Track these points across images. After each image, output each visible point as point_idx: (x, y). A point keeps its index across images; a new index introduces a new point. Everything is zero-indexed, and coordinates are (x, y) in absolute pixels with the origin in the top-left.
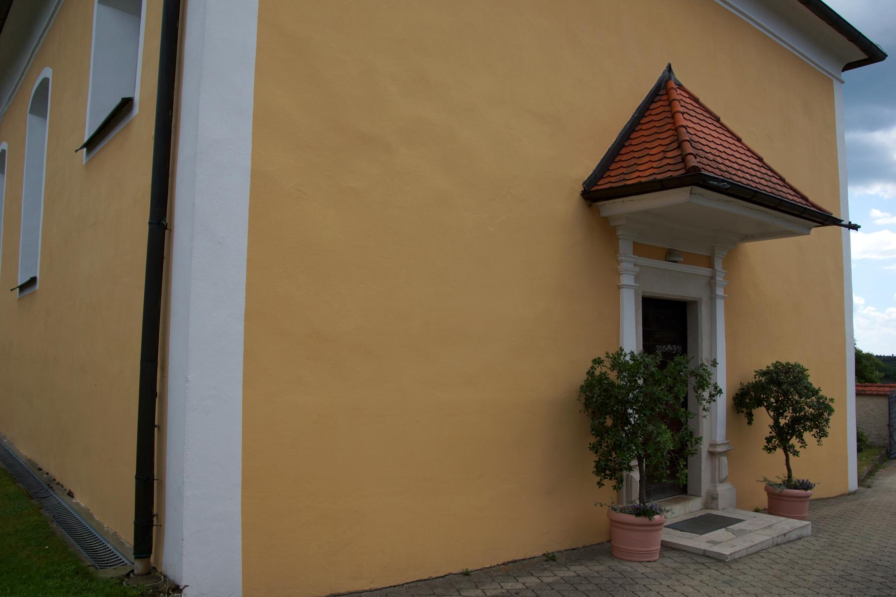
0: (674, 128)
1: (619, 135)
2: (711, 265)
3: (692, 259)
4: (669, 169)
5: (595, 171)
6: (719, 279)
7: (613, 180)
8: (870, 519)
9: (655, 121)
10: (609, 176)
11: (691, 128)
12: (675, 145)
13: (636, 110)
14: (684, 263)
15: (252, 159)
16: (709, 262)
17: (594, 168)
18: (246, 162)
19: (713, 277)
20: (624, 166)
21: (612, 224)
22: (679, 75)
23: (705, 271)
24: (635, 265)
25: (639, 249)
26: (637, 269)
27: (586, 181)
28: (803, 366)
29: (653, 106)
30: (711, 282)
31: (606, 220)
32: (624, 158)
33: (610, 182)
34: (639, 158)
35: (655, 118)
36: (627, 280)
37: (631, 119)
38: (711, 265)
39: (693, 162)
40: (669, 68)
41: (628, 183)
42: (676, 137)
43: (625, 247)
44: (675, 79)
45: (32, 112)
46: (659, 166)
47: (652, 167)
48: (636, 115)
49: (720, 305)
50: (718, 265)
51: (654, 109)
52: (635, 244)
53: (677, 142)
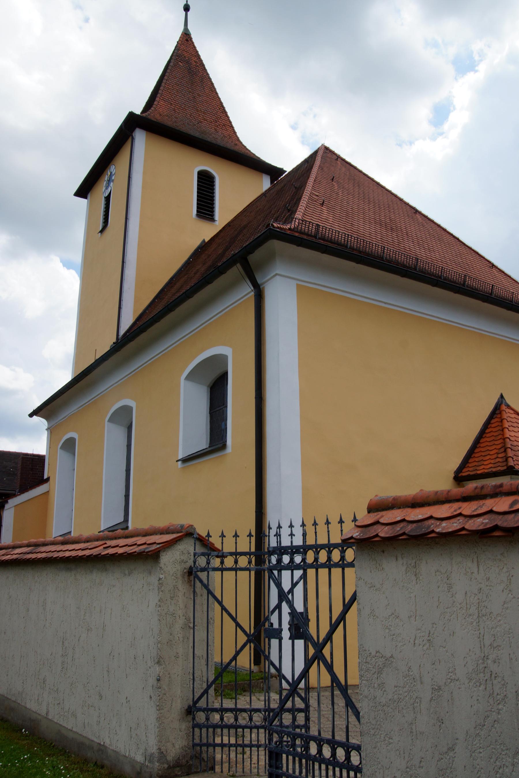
0: (503, 438)
1: (473, 441)
4: (499, 465)
5: (460, 465)
7: (470, 469)
9: (494, 432)
10: (468, 466)
11: (512, 437)
12: (503, 450)
13: (483, 425)
15: (302, 482)
17: (460, 462)
18: (299, 484)
20: (482, 451)
22: (509, 400)
27: (456, 471)
29: (493, 421)
32: (476, 455)
33: (469, 471)
34: (484, 456)
35: (494, 430)
37: (480, 431)
39: (511, 463)
40: (502, 396)
41: (479, 472)
42: (504, 445)
44: (506, 402)
45: (110, 420)
46: (494, 463)
47: (491, 463)
48: (483, 428)
51: (483, 443)
53: (503, 448)
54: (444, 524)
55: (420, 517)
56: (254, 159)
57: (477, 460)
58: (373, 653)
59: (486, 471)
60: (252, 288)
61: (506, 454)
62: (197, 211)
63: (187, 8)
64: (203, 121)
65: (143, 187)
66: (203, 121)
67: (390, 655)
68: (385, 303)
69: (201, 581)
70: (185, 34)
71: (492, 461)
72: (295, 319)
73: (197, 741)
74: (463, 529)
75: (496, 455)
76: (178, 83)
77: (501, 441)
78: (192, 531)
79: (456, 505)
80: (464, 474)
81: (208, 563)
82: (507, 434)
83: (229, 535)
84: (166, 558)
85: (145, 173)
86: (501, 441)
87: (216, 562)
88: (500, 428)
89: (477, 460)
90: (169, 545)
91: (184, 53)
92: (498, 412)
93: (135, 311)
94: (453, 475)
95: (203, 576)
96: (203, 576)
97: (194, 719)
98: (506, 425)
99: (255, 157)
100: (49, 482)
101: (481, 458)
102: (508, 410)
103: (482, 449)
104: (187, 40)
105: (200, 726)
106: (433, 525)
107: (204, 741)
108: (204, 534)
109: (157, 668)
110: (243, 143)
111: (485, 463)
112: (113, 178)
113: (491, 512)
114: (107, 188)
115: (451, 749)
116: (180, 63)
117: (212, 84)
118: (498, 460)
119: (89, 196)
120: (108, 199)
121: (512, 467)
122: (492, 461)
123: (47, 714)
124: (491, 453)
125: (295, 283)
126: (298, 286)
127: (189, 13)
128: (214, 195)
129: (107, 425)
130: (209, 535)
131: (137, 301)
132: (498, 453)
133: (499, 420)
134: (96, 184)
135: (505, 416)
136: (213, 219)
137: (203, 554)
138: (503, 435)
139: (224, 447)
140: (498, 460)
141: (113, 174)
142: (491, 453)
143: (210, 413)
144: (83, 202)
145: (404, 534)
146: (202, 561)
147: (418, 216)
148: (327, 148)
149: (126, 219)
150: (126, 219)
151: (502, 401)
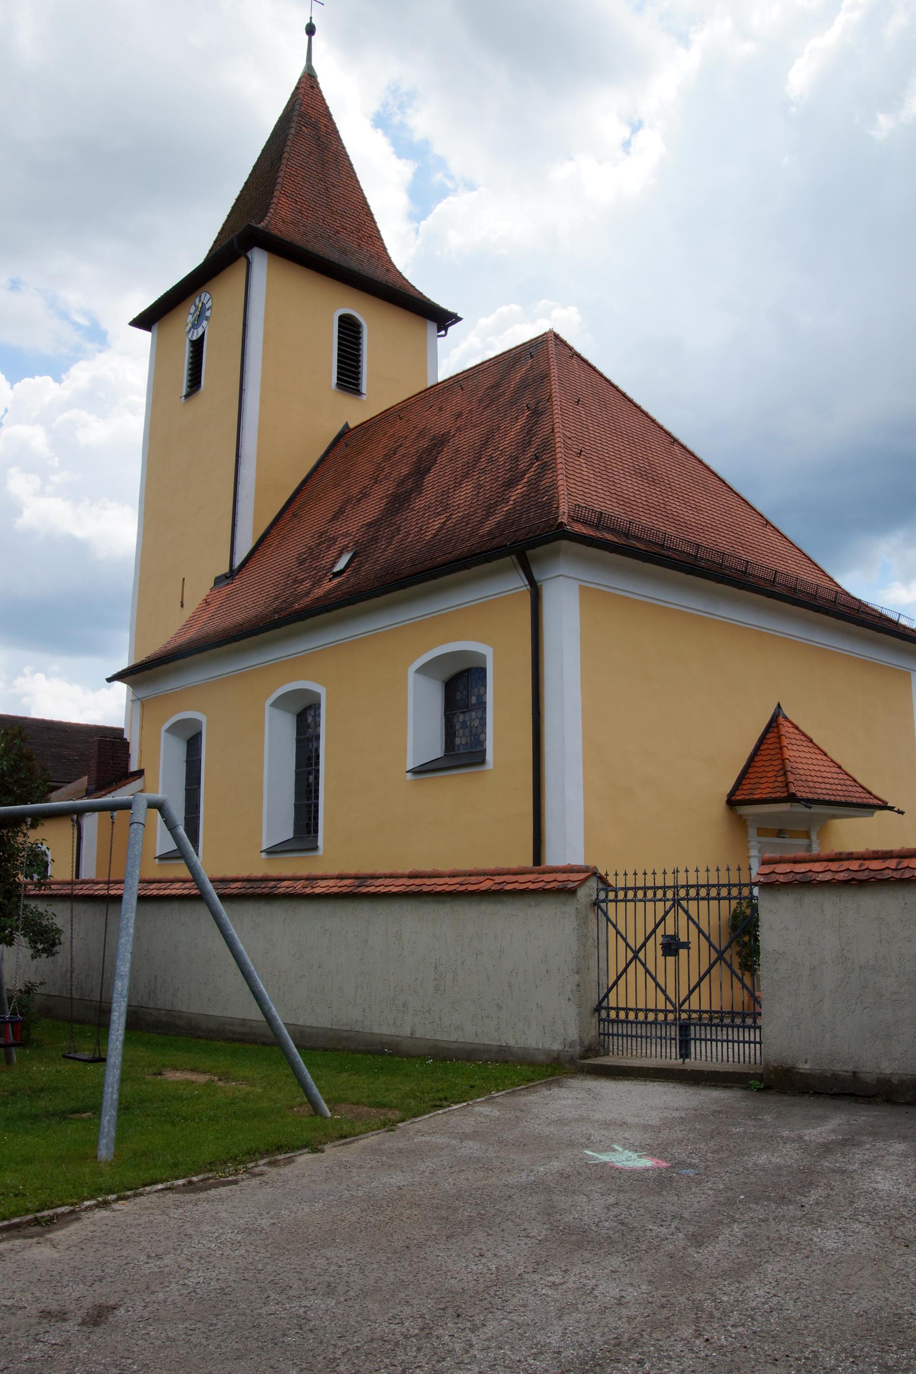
2: (809, 837)
3: (795, 834)
7: (745, 792)
12: (781, 772)
14: (790, 837)
16: (807, 835)
18: (581, 810)
21: (744, 818)
22: (786, 711)
23: (804, 842)
24: (759, 842)
25: (761, 832)
26: (760, 845)
31: (740, 816)
35: (771, 747)
36: (754, 852)
38: (808, 836)
39: (793, 790)
40: (779, 706)
43: (752, 832)
50: (814, 837)
52: (758, 829)
54: (821, 875)
55: (803, 870)
56: (423, 302)
57: (752, 781)
58: (771, 951)
59: (764, 796)
60: (527, 583)
61: (787, 778)
62: (338, 379)
63: (311, 30)
64: (341, 230)
65: (265, 342)
66: (341, 230)
67: (782, 951)
68: (665, 602)
69: (602, 910)
70: (309, 75)
71: (770, 785)
72: (578, 627)
73: (602, 1031)
74: (834, 879)
75: (774, 778)
76: (304, 164)
77: (779, 762)
78: (596, 871)
79: (825, 864)
80: (738, 798)
81: (607, 896)
82: (787, 753)
83: (630, 874)
84: (581, 892)
85: (267, 318)
86: (779, 762)
87: (611, 895)
88: (778, 746)
89: (752, 781)
90: (583, 882)
91: (309, 110)
92: (774, 725)
93: (254, 530)
94: (726, 799)
95: (603, 905)
96: (603, 905)
97: (599, 1015)
98: (785, 742)
99: (424, 299)
100: (143, 778)
101: (757, 780)
102: (786, 723)
103: (758, 770)
105: (604, 1020)
106: (814, 876)
107: (606, 1032)
108: (603, 874)
109: (577, 977)
111: (762, 786)
112: (208, 314)
113: (848, 869)
114: (195, 326)
115: (821, 1001)
116: (304, 128)
117: (351, 165)
118: (777, 784)
119: (155, 327)
120: (197, 346)
121: (794, 795)
122: (770, 785)
123: (412, 1034)
124: (769, 775)
125: (578, 583)
126: (581, 587)
127: (313, 38)
128: (361, 353)
129: (268, 712)
130: (607, 875)
131: (257, 514)
132: (776, 776)
133: (776, 735)
134: (171, 313)
135: (783, 731)
136: (358, 391)
137: (603, 889)
138: (782, 754)
139: (482, 762)
140: (777, 784)
141: (207, 306)
142: (769, 775)
143: (445, 715)
144: (145, 337)
145: (796, 880)
146: (602, 895)
147: (676, 448)
148: (556, 336)
151: (779, 712)
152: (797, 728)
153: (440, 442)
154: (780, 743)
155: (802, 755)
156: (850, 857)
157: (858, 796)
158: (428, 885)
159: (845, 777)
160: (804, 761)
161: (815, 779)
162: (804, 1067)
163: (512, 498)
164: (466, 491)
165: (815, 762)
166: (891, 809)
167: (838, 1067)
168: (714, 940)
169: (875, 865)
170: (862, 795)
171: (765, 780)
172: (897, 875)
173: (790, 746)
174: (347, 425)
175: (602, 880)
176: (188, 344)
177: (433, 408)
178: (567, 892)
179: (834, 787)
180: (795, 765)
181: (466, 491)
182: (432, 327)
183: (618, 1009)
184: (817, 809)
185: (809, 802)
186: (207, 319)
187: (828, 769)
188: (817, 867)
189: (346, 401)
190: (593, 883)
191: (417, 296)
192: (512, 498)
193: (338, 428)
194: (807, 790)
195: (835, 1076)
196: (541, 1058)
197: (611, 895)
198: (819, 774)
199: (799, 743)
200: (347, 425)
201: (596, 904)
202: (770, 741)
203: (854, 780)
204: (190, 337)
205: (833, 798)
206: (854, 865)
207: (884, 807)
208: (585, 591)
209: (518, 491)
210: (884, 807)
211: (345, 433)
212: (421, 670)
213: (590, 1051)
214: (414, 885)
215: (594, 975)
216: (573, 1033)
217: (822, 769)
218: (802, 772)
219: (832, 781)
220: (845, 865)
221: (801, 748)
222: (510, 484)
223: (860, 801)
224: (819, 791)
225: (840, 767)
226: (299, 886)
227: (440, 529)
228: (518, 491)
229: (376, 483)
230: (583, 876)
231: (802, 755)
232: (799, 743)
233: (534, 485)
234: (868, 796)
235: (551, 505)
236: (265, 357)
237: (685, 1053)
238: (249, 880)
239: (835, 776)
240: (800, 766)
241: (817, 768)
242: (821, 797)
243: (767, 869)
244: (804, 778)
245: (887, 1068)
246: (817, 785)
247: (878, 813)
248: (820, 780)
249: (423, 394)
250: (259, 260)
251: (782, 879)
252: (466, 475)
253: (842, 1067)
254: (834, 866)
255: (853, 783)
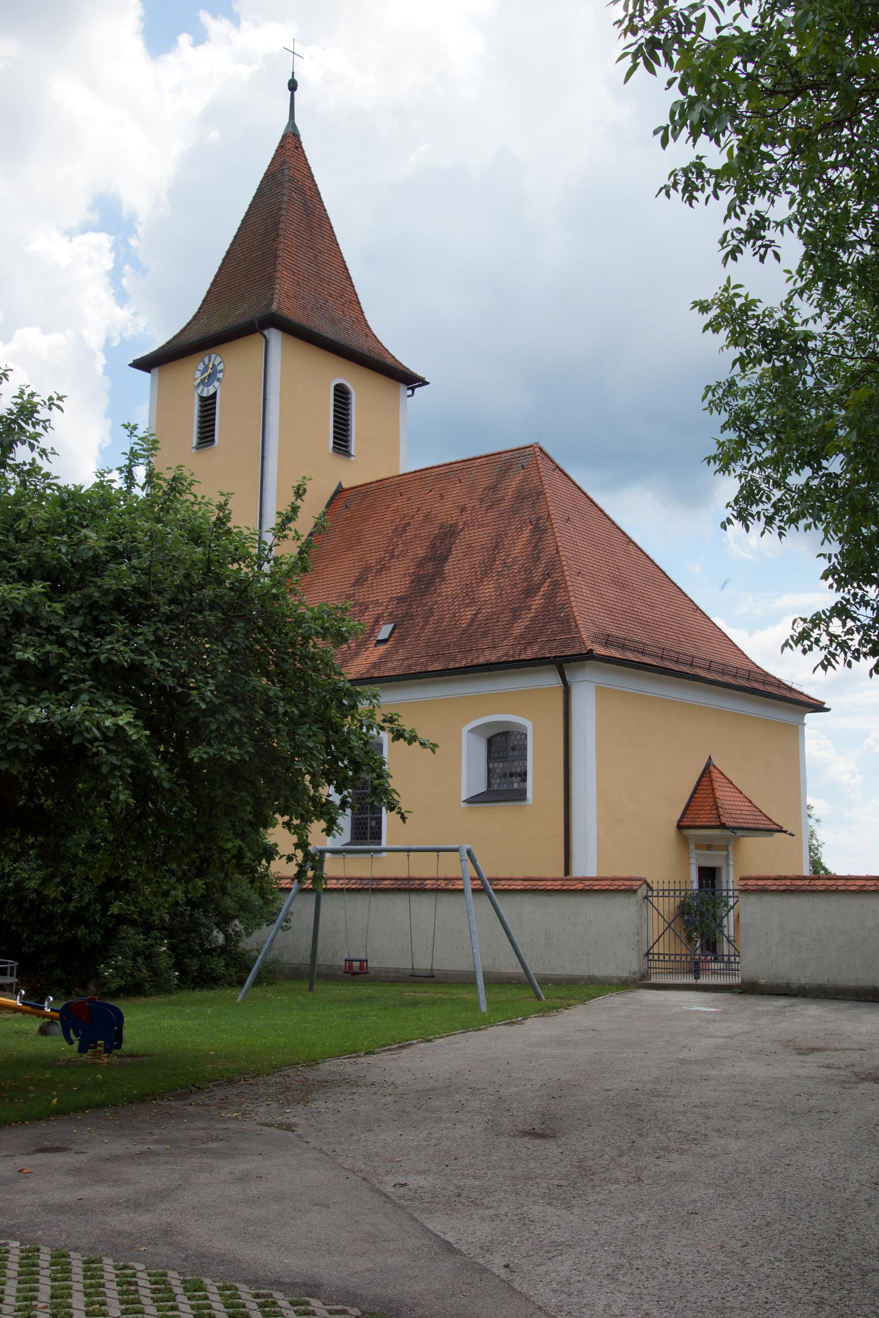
2: (727, 850)
6: (731, 856)
8: (194, 1288)
12: (714, 807)
19: (728, 856)
22: (715, 761)
25: (698, 847)
28: (711, 140)
30: (727, 858)
31: (685, 836)
36: (693, 861)
40: (710, 758)
43: (692, 846)
49: (731, 869)
63: (293, 86)
82: (718, 794)
84: (639, 892)
85: (281, 393)
90: (640, 885)
95: (650, 899)
96: (650, 899)
98: (716, 785)
102: (715, 771)
104: (297, 148)
110: (373, 330)
112: (220, 375)
119: (155, 371)
120: (208, 405)
124: (706, 808)
136: (347, 452)
142: (706, 808)
147: (631, 546)
149: (263, 457)
150: (263, 457)
152: (722, 774)
153: (449, 534)
154: (712, 785)
155: (727, 794)
156: (785, 878)
157: (763, 824)
158: (541, 885)
159: (755, 809)
160: (728, 798)
161: (736, 812)
162: (762, 981)
163: (534, 607)
164: (487, 590)
165: (735, 799)
166: (785, 832)
167: (779, 981)
168: (666, 918)
169: (798, 883)
170: (766, 822)
171: (703, 812)
172: (809, 888)
173: (719, 788)
174: (340, 484)
175: (650, 888)
176: (196, 403)
177: (432, 493)
178: (632, 891)
179: (748, 817)
180: (723, 802)
181: (487, 590)
182: (403, 387)
183: (659, 954)
184: (739, 833)
185: (733, 829)
186: (219, 380)
187: (743, 804)
188: (769, 882)
189: (339, 462)
190: (644, 887)
191: (403, 369)
192: (534, 607)
193: (333, 488)
194: (732, 820)
195: (778, 986)
196: (616, 981)
197: (655, 893)
198: (738, 808)
199: (724, 785)
200: (340, 484)
201: (646, 897)
202: (704, 784)
203: (761, 812)
204: (199, 391)
205: (748, 825)
206: (788, 882)
207: (781, 830)
208: (600, 692)
209: (537, 602)
210: (781, 830)
211: (340, 491)
212: (473, 731)
213: (645, 976)
214: (529, 885)
215: (645, 936)
216: (635, 967)
217: (740, 804)
218: (727, 807)
219: (746, 813)
220: (783, 882)
221: (726, 789)
222: (530, 592)
223: (765, 826)
224: (739, 820)
225: (751, 802)
226: (443, 884)
227: (473, 620)
228: (537, 602)
229: (393, 557)
230: (640, 883)
231: (727, 794)
232: (724, 785)
233: (551, 597)
234: (770, 822)
235: (567, 623)
236: (281, 428)
237: (697, 978)
238: (396, 879)
239: (748, 808)
240: (726, 802)
241: (736, 803)
242: (741, 825)
243: (743, 882)
244: (729, 811)
245: (803, 981)
246: (737, 816)
247: (777, 834)
248: (739, 812)
249: (418, 474)
250: (275, 337)
251: (751, 888)
252: (485, 574)
253: (781, 981)
254: (778, 882)
255: (759, 814)
